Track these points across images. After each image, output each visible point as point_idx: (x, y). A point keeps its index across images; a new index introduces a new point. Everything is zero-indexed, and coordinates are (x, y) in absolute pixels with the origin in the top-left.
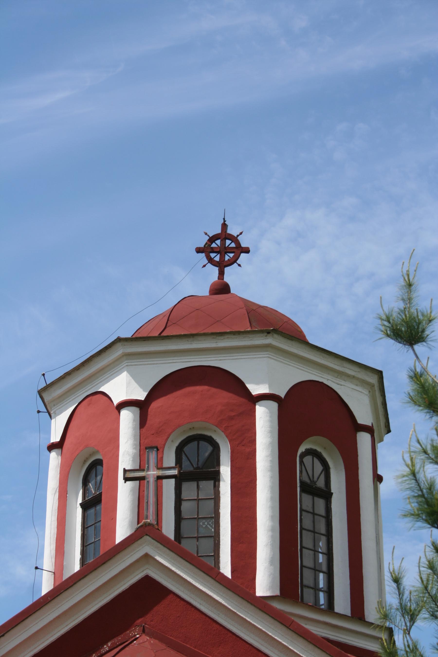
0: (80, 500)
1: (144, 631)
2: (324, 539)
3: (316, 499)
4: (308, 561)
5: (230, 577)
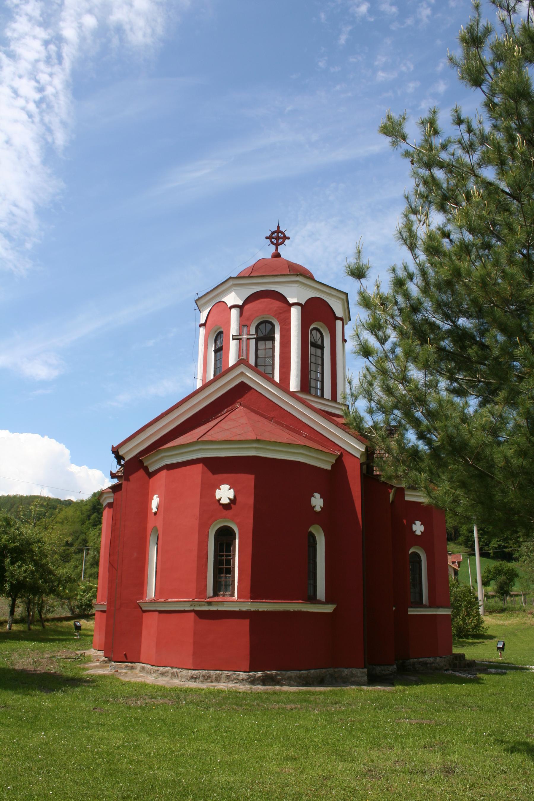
0: (213, 349)
1: (241, 405)
2: (320, 367)
3: (317, 349)
4: (313, 376)
5: (279, 382)
